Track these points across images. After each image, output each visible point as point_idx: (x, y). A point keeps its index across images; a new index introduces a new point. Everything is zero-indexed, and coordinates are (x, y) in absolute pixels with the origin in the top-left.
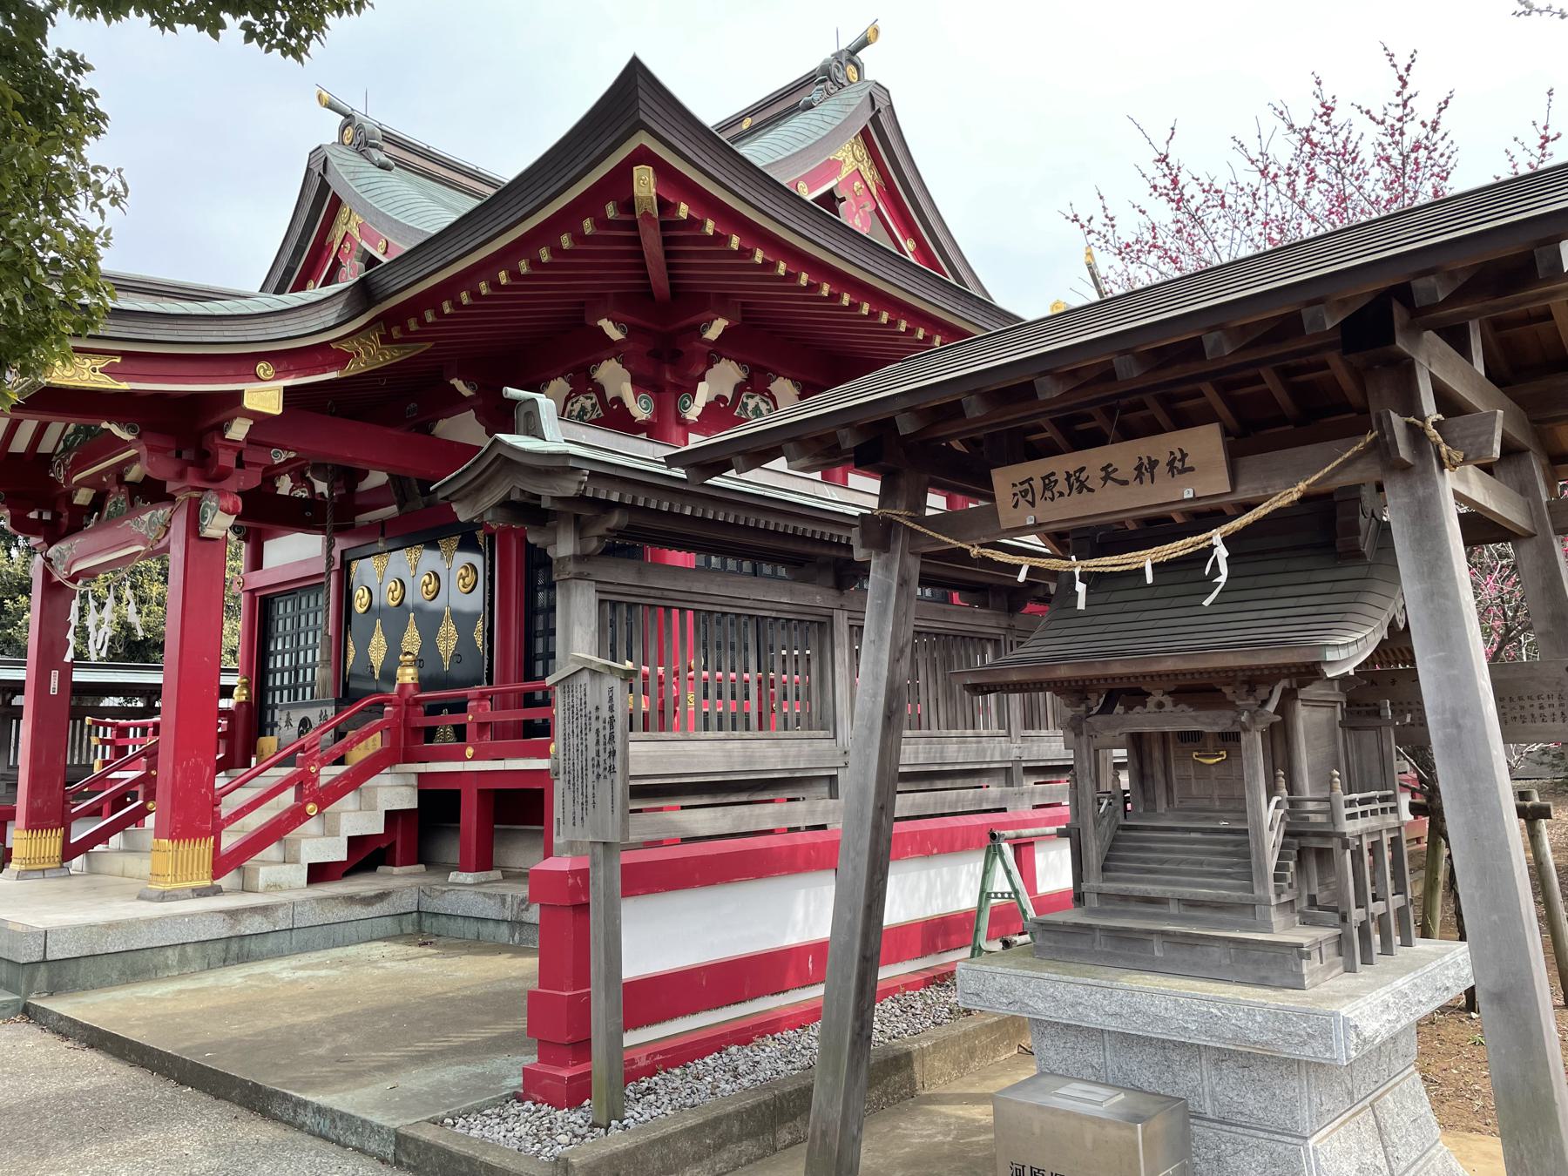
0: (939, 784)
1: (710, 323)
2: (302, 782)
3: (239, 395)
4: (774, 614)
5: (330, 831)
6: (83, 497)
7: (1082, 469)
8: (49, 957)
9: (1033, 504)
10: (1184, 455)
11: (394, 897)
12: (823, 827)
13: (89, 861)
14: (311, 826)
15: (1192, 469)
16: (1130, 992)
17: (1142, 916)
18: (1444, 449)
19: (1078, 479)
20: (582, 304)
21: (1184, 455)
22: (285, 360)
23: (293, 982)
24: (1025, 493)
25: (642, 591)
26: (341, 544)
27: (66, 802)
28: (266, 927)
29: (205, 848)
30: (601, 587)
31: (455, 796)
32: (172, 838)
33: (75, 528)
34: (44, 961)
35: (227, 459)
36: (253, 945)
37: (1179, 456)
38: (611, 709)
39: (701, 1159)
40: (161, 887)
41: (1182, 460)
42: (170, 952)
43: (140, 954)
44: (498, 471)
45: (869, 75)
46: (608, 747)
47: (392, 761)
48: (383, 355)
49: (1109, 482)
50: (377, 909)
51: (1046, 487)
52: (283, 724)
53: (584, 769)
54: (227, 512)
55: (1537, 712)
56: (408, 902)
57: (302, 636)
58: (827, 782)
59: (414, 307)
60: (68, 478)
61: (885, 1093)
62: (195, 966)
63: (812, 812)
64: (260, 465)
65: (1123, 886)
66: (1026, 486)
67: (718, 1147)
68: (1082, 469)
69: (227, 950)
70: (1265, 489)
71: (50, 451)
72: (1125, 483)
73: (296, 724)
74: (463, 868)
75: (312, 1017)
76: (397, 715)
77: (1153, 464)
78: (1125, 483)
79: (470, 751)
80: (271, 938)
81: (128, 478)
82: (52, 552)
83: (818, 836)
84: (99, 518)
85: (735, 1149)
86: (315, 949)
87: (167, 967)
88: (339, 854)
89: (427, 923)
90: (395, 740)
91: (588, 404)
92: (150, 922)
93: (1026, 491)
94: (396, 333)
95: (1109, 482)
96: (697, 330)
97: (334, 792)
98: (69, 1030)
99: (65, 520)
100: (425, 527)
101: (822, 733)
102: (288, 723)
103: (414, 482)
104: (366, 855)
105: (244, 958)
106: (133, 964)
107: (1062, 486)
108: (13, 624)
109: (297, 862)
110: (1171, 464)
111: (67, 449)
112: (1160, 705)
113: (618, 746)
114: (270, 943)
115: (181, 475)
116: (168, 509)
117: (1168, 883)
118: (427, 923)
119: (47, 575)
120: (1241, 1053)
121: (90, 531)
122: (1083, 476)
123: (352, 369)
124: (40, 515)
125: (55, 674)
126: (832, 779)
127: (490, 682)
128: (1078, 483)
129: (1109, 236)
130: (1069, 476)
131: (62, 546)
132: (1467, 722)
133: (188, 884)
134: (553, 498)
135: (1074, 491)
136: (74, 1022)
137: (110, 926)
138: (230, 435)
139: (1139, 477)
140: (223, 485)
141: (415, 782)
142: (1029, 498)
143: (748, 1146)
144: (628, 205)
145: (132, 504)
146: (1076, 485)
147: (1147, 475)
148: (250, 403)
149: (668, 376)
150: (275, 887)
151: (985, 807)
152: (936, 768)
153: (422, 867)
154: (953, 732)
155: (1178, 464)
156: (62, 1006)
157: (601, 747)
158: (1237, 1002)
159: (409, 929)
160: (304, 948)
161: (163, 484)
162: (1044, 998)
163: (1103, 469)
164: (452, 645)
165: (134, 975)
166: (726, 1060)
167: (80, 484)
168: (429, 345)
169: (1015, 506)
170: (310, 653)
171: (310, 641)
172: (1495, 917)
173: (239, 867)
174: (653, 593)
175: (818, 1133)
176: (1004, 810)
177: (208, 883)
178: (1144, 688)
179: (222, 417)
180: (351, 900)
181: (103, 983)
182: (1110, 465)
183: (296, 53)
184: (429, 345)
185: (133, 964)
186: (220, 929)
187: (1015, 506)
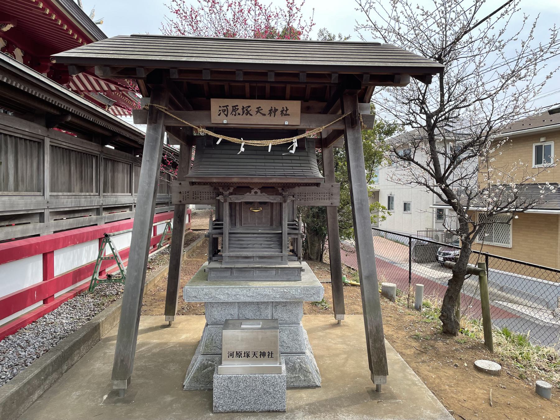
0: (77, 215)
7: (249, 107)
9: (227, 116)
10: (287, 110)
12: (39, 235)
15: (289, 115)
16: (256, 288)
17: (259, 263)
18: (362, 124)
19: (247, 110)
21: (287, 110)
24: (224, 111)
37: (285, 109)
39: (40, 386)
41: (286, 111)
49: (259, 114)
51: (233, 110)
55: (323, 197)
61: (93, 341)
63: (35, 229)
65: (238, 253)
66: (225, 108)
67: (45, 379)
68: (249, 107)
70: (309, 126)
72: (264, 115)
77: (276, 110)
78: (264, 115)
85: (50, 378)
93: (225, 110)
95: (259, 114)
101: (38, 193)
107: (240, 111)
110: (282, 111)
112: (256, 193)
117: (252, 251)
120: (283, 302)
122: (249, 109)
128: (246, 111)
129: (182, 5)
130: (243, 108)
132: (364, 203)
135: (244, 114)
139: (270, 114)
142: (226, 113)
143: (55, 375)
146: (246, 112)
147: (273, 114)
151: (92, 224)
152: (77, 209)
154: (83, 194)
155: (284, 112)
158: (292, 287)
162: (224, 294)
163: (257, 108)
166: (10, 342)
169: (219, 115)
172: (368, 256)
175: (119, 361)
176: (96, 225)
178: (251, 187)
182: (260, 107)
187: (219, 115)
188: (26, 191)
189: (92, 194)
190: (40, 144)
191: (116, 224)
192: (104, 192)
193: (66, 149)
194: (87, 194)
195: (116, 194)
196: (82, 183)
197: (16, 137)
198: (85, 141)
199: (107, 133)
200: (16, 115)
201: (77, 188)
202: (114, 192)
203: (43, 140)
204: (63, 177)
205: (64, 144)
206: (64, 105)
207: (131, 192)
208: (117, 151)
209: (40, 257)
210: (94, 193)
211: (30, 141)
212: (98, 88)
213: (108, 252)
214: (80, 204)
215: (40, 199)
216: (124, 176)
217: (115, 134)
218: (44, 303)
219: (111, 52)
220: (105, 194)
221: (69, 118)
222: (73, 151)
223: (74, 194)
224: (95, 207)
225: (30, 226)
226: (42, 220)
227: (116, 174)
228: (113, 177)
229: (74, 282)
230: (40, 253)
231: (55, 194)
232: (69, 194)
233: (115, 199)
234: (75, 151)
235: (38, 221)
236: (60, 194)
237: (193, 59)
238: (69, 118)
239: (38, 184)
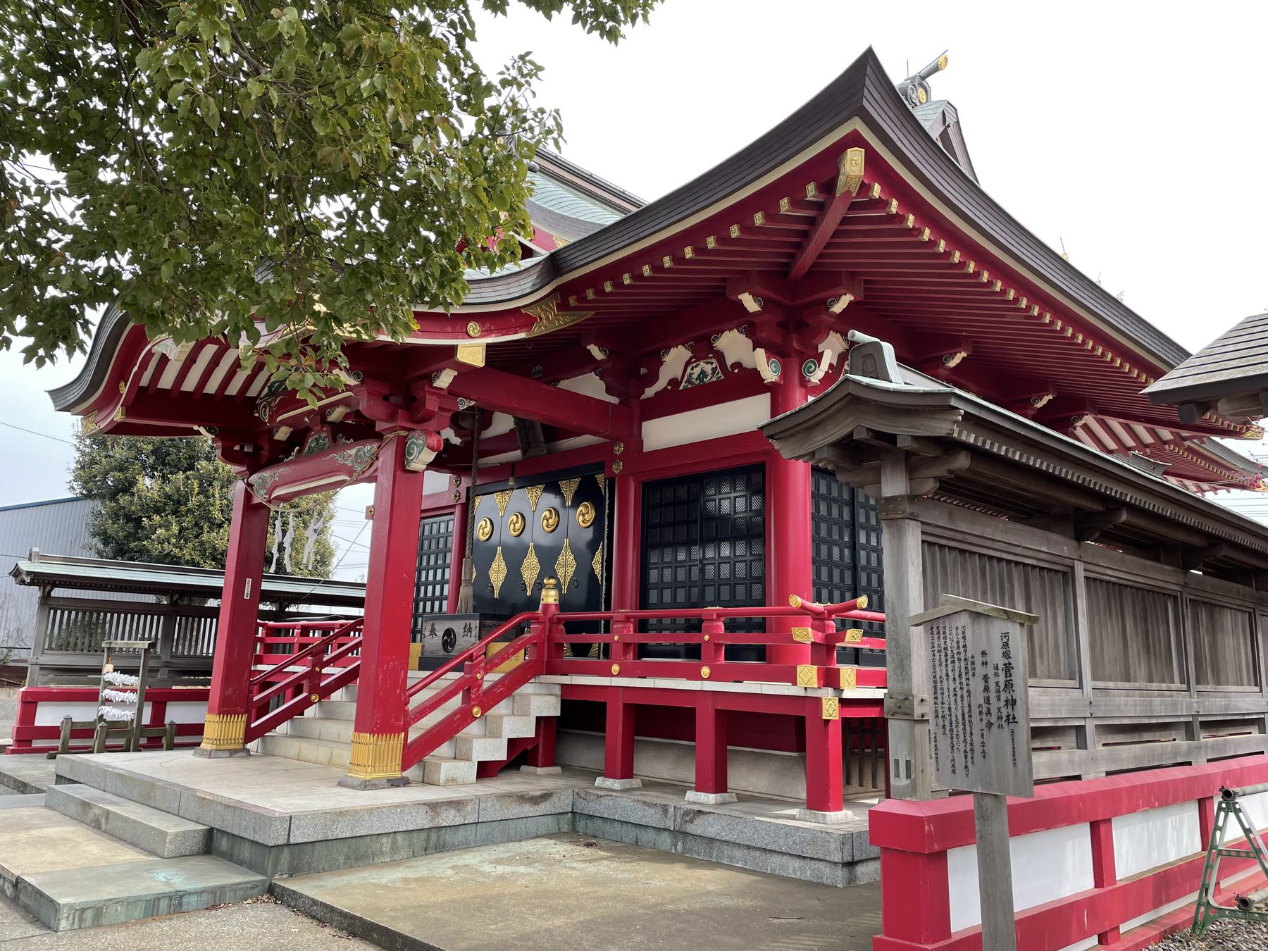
1: (838, 298)
2: (468, 688)
3: (452, 350)
4: (1035, 563)
5: (493, 733)
6: (282, 434)
8: (292, 841)
11: (554, 798)
12: (1078, 778)
13: (264, 743)
14: (473, 728)
20: (724, 280)
22: (491, 320)
23: (502, 878)
25: (947, 534)
26: (466, 482)
27: (251, 692)
28: (458, 821)
29: (394, 745)
30: (929, 529)
31: (601, 707)
32: (372, 732)
33: (273, 461)
34: (288, 845)
35: (432, 404)
36: (447, 836)
38: (1007, 655)
40: (362, 776)
42: (384, 840)
43: (362, 840)
44: (838, 411)
45: (935, 96)
46: (1003, 696)
47: (538, 673)
48: (558, 320)
50: (543, 808)
52: (427, 633)
53: (967, 717)
54: (432, 449)
56: (563, 802)
57: (425, 558)
58: (1073, 733)
59: (594, 279)
60: (272, 418)
62: (404, 854)
63: (1071, 762)
64: (448, 410)
69: (428, 839)
71: (255, 395)
73: (440, 634)
74: (608, 774)
75: (559, 922)
76: (543, 630)
79: (615, 668)
80: (461, 831)
81: (330, 419)
82: (254, 478)
83: (1072, 788)
84: (299, 452)
86: (494, 843)
87: (382, 853)
88: (501, 755)
89: (581, 824)
90: (540, 655)
91: (708, 368)
92: (371, 811)
94: (572, 301)
96: (824, 305)
97: (491, 699)
98: (323, 915)
99: (265, 453)
100: (539, 472)
102: (433, 632)
103: (539, 431)
104: (521, 755)
105: (441, 848)
106: (355, 850)
108: (147, 538)
109: (468, 759)
111: (270, 394)
113: (1018, 695)
114: (460, 835)
115: (392, 417)
116: (375, 446)
118: (581, 824)
119: (248, 496)
121: (292, 462)
123: (537, 331)
124: (242, 448)
125: (249, 581)
126: (1080, 730)
127: (608, 608)
131: (266, 474)
133: (384, 775)
134: (916, 438)
136: (333, 909)
137: (341, 813)
138: (438, 384)
140: (425, 425)
141: (559, 693)
144: (828, 187)
145: (334, 440)
148: (462, 356)
149: (795, 344)
150: (452, 781)
152: (1146, 721)
153: (557, 769)
154: (1155, 686)
156: (307, 888)
157: (993, 695)
159: (565, 828)
160: (487, 841)
161: (372, 424)
164: (571, 571)
165: (356, 860)
167: (283, 423)
168: (591, 313)
170: (431, 572)
171: (432, 562)
173: (420, 761)
174: (958, 536)
176: (1189, 763)
177: (398, 774)
179: (433, 368)
180: (522, 798)
181: (332, 868)
183: (613, 35)
184: (591, 313)
185: (355, 850)
186: (422, 820)
188: (1049, 677)
189: (1173, 686)
190: (1067, 576)
191: (1233, 764)
192: (1198, 683)
193: (1114, 584)
194: (1164, 686)
195: (1224, 688)
196: (1149, 660)
197: (1026, 565)
198: (1149, 563)
199: (1196, 541)
200: (1011, 518)
201: (1142, 672)
202: (1218, 683)
203: (1072, 568)
204: (1112, 649)
205: (1110, 572)
206: (1116, 490)
207: (1257, 682)
208: (1207, 577)
209: (1085, 829)
210: (1176, 685)
211: (1049, 570)
212: (1130, 442)
213: (1231, 832)
214: (1152, 711)
215: (1076, 694)
216: (1238, 643)
217: (1215, 541)
218: (1100, 942)
219: (1235, 363)
220: (1201, 687)
221: (1124, 517)
222: (1126, 586)
223: (1137, 685)
224: (1182, 720)
225: (1063, 755)
226: (1082, 745)
227: (1219, 637)
228: (1214, 645)
229: (1158, 903)
230: (1085, 821)
231: (1101, 684)
232: (1127, 685)
233: (1224, 701)
234: (1131, 587)
235: (1074, 745)
236: (1111, 685)
237: (1250, 372)
238: (1124, 517)
239: (1070, 665)
